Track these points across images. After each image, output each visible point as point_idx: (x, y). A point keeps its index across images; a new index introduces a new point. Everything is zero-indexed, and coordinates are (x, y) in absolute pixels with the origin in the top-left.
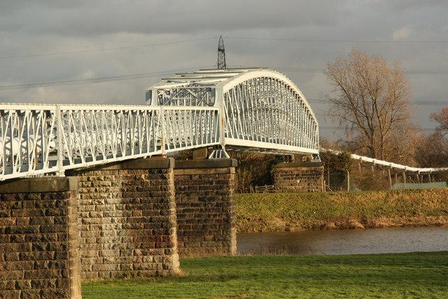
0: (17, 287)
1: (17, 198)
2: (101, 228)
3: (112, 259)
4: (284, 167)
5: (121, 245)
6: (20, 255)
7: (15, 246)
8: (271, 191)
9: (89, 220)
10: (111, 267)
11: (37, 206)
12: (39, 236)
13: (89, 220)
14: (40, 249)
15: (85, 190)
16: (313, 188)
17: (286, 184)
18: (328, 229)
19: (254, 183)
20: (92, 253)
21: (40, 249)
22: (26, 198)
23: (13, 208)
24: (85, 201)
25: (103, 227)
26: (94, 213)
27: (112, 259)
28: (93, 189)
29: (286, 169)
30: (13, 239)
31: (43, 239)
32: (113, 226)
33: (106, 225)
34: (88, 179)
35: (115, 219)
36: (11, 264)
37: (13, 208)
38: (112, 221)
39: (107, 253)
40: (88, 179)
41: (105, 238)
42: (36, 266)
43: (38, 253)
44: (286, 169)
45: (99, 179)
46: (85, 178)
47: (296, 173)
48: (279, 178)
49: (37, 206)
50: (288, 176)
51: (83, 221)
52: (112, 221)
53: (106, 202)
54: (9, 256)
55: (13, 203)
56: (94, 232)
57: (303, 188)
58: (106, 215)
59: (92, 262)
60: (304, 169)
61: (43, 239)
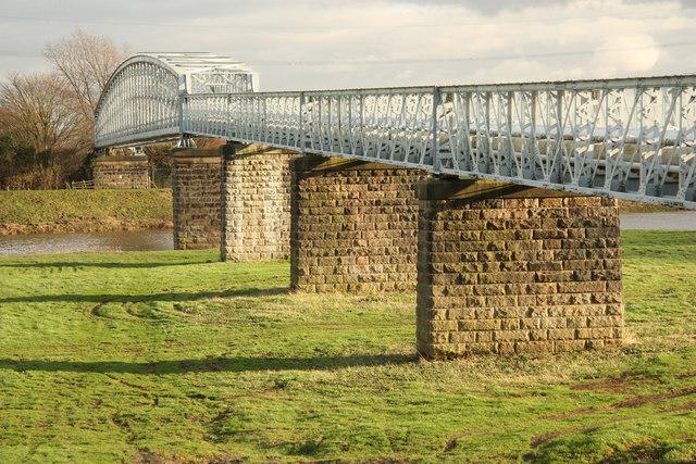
0: (387, 252)
1: (386, 174)
2: (262, 211)
3: (274, 241)
4: (103, 161)
5: (283, 227)
6: (389, 225)
7: (384, 216)
8: (91, 187)
9: (251, 203)
10: (273, 248)
11: (403, 181)
12: (406, 208)
13: (251, 203)
14: (407, 219)
15: (247, 173)
16: (137, 183)
17: (107, 180)
18: (167, 227)
19: (70, 179)
20: (255, 235)
21: (407, 219)
22: (394, 174)
23: (383, 182)
24: (247, 185)
25: (265, 209)
26: (256, 197)
27: (274, 241)
28: (254, 173)
29: (106, 163)
30: (383, 211)
31: (409, 211)
32: (275, 209)
33: (267, 206)
34: (250, 163)
35: (277, 202)
36: (381, 233)
37: (383, 182)
38: (274, 204)
39: (269, 235)
40: (250, 163)
41: (266, 221)
42: (402, 235)
43: (405, 223)
44: (106, 163)
45: (260, 163)
46: (246, 161)
47: (118, 167)
48: (99, 173)
49: (403, 181)
50: (110, 171)
51: (245, 204)
52: (274, 204)
53: (267, 185)
54: (379, 226)
55: (382, 178)
56: (255, 214)
57: (126, 184)
58: (267, 198)
59: (254, 244)
60: (128, 163)
61: (409, 211)
